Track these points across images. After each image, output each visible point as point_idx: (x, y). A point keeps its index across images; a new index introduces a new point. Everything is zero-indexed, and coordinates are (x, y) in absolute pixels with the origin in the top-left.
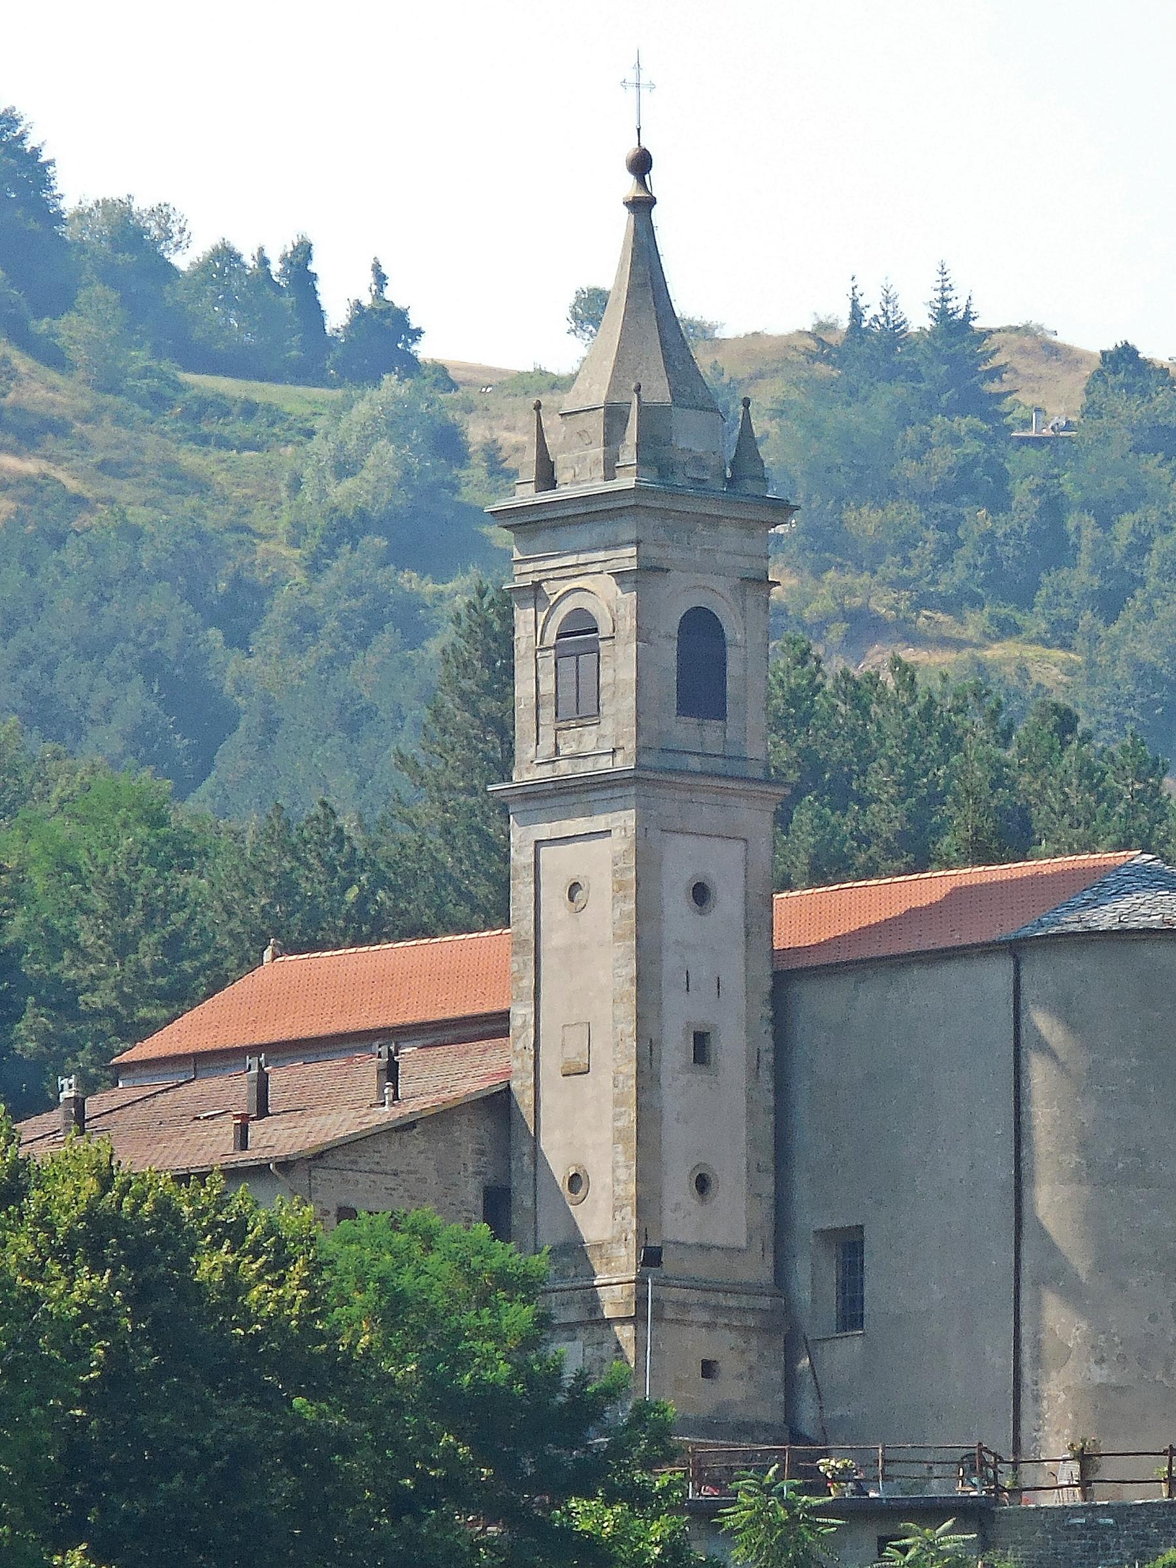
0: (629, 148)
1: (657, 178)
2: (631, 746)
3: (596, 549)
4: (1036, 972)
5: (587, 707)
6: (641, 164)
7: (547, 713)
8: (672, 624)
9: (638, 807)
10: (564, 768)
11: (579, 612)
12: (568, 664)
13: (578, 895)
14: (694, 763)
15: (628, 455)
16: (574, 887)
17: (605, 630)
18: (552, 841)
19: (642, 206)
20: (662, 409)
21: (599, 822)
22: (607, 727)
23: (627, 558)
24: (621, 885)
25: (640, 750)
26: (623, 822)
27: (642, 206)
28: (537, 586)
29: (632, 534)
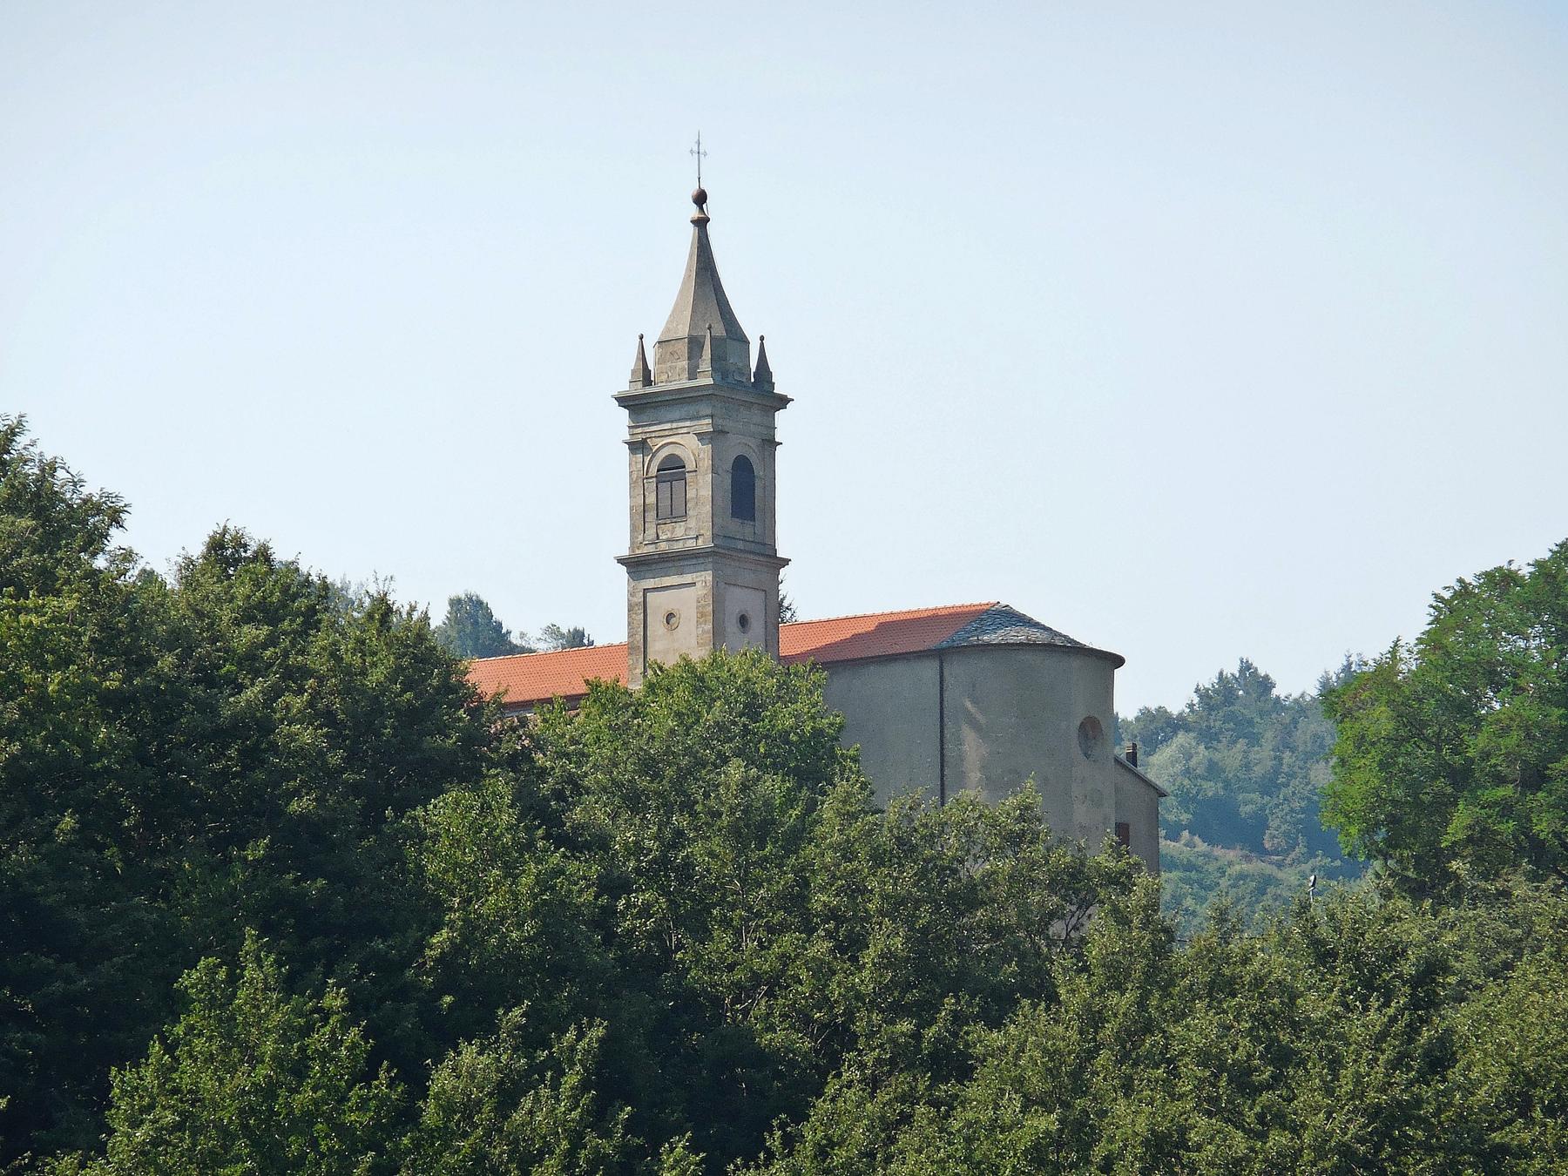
0: (694, 190)
1: (711, 207)
2: (709, 533)
3: (685, 419)
4: (957, 671)
5: (679, 510)
6: (701, 198)
7: (651, 516)
8: (729, 466)
9: (715, 571)
10: (663, 546)
11: (672, 457)
12: (665, 487)
13: (673, 620)
14: (740, 545)
15: (705, 364)
16: (670, 616)
17: (690, 466)
18: (655, 589)
19: (701, 223)
20: (721, 339)
21: (688, 578)
22: (692, 523)
23: (705, 425)
24: (703, 615)
25: (714, 536)
26: (703, 579)
27: (701, 223)
28: (644, 441)
29: (709, 412)
